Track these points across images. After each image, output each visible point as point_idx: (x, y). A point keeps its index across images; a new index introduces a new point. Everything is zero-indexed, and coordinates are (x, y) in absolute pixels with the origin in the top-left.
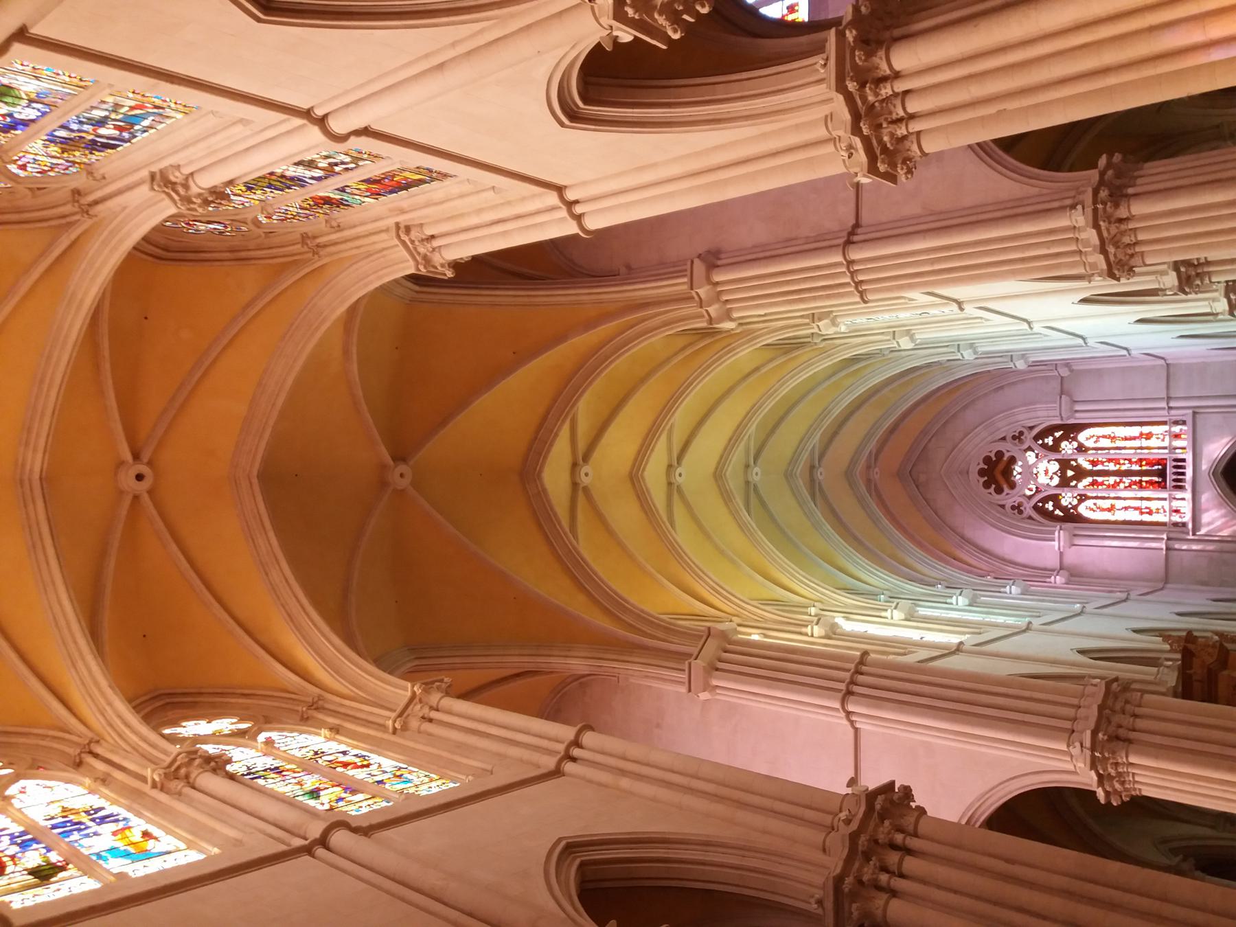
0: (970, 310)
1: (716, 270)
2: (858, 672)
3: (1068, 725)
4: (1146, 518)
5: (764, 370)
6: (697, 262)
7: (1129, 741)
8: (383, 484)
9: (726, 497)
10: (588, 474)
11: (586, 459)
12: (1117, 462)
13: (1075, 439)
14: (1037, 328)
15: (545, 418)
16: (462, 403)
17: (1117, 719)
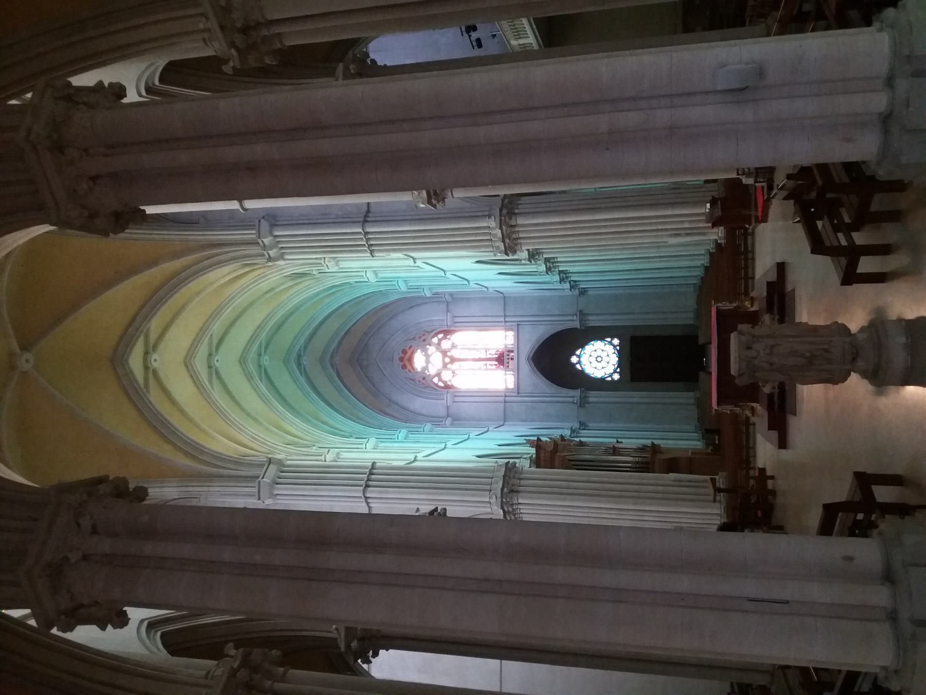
0: (419, 263)
1: (275, 228)
2: (371, 474)
3: (488, 487)
6: (262, 221)
7: (518, 492)
8: (12, 368)
9: (249, 377)
11: (155, 347)
14: (448, 275)
15: (133, 320)
16: (74, 307)
17: (512, 481)
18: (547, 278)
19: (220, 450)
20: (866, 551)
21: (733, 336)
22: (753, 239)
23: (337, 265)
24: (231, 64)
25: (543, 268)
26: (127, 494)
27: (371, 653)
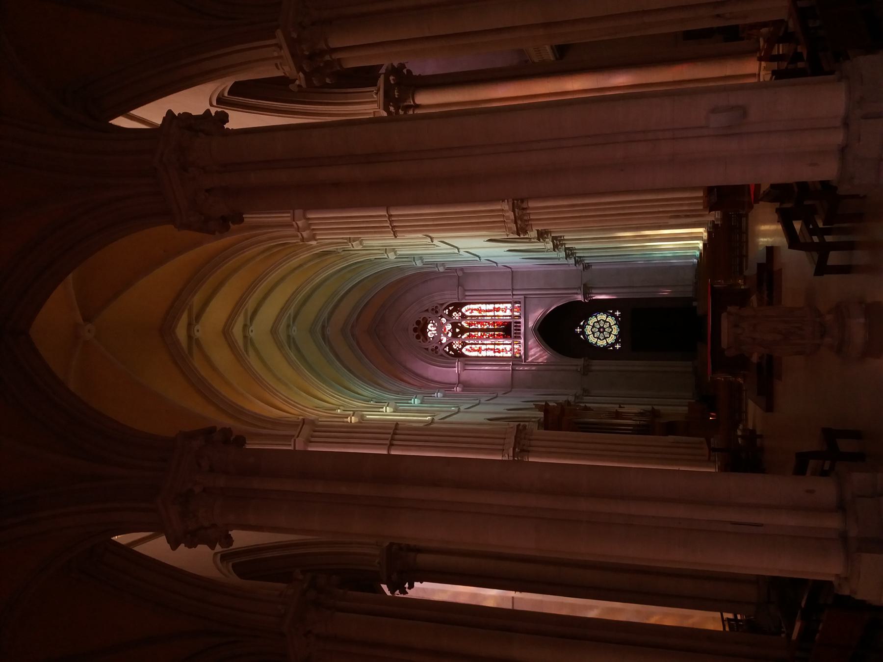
0: (436, 242)
2: (395, 434)
3: (501, 447)
4: (497, 354)
5: (306, 266)
7: (528, 451)
9: (280, 347)
10: (294, 331)
12: (482, 324)
13: (460, 311)
18: (554, 255)
19: (257, 411)
20: (825, 490)
21: (724, 315)
22: (747, 220)
23: (361, 243)
24: (297, 82)
25: (550, 245)
26: (232, 440)
27: (407, 585)
